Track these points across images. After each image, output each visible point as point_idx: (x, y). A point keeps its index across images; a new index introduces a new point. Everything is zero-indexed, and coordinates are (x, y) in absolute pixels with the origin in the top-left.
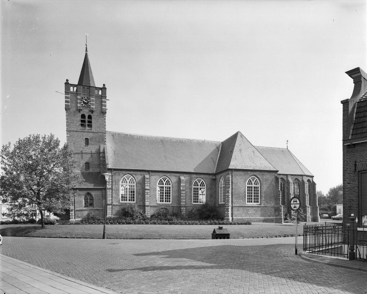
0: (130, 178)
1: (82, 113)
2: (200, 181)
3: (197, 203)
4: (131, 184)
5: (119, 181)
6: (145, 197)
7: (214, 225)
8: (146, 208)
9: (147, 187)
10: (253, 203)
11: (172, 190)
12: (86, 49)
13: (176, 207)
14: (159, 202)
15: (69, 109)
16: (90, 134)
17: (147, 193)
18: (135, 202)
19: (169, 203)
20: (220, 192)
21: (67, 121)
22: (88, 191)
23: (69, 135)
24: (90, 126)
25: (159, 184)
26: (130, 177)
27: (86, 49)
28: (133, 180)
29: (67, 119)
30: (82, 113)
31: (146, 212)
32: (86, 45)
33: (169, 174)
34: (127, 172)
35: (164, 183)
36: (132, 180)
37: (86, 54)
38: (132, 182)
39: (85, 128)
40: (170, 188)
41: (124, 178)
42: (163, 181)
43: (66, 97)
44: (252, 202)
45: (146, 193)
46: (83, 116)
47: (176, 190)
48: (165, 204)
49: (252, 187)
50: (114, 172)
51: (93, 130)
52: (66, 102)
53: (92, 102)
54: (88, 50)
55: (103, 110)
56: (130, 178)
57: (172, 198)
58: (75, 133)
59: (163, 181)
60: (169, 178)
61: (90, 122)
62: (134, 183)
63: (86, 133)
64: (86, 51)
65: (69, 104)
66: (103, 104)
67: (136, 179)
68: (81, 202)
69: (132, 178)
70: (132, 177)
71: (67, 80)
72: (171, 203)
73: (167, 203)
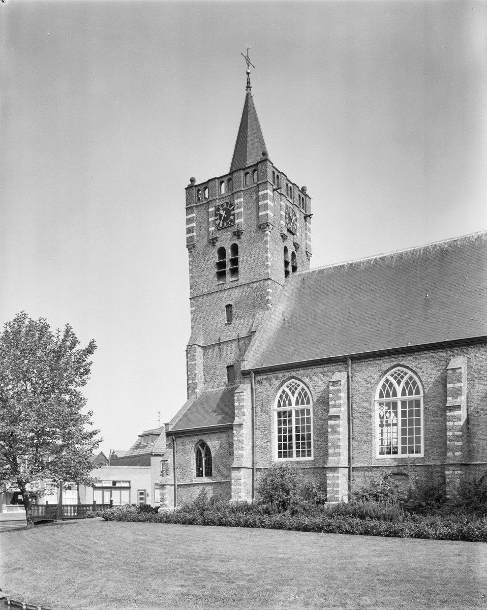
0: (406, 378)
1: (218, 245)
2: (402, 377)
3: (414, 455)
4: (407, 397)
5: (269, 401)
6: (326, 440)
7: (218, 527)
8: (328, 475)
9: (334, 409)
10: (295, 458)
11: (425, 409)
12: (248, 83)
13: (438, 469)
14: (276, 459)
15: (194, 246)
16: (236, 290)
17: (332, 427)
18: (421, 455)
19: (414, 455)
20: (422, 417)
21: (191, 275)
22: (200, 437)
23: (194, 308)
24: (235, 271)
25: (381, 396)
26: (406, 374)
27: (248, 83)
28: (415, 383)
29: (191, 271)
30: (218, 245)
31: (328, 489)
32: (248, 73)
33: (302, 372)
34: (288, 374)
35: (399, 390)
36: (303, 395)
37: (248, 98)
38: (284, 402)
39: (226, 281)
40: (418, 403)
41: (387, 381)
42: (395, 383)
43: (189, 221)
44: (291, 456)
45: (330, 430)
46: (222, 252)
47: (436, 409)
48: (297, 463)
49: (290, 412)
50: (258, 378)
51: (243, 277)
52: (189, 230)
53: (237, 211)
54: (251, 85)
55: (260, 219)
56: (406, 378)
57: (425, 438)
58: (206, 298)
59: (395, 383)
60: (411, 370)
61: (235, 262)
62: (418, 392)
63: (227, 292)
64: (248, 87)
65: (194, 234)
66: (260, 203)
67: (311, 389)
68: (187, 464)
69: (411, 378)
70: (410, 373)
71: (192, 180)
72: (421, 455)
73: (301, 459)
